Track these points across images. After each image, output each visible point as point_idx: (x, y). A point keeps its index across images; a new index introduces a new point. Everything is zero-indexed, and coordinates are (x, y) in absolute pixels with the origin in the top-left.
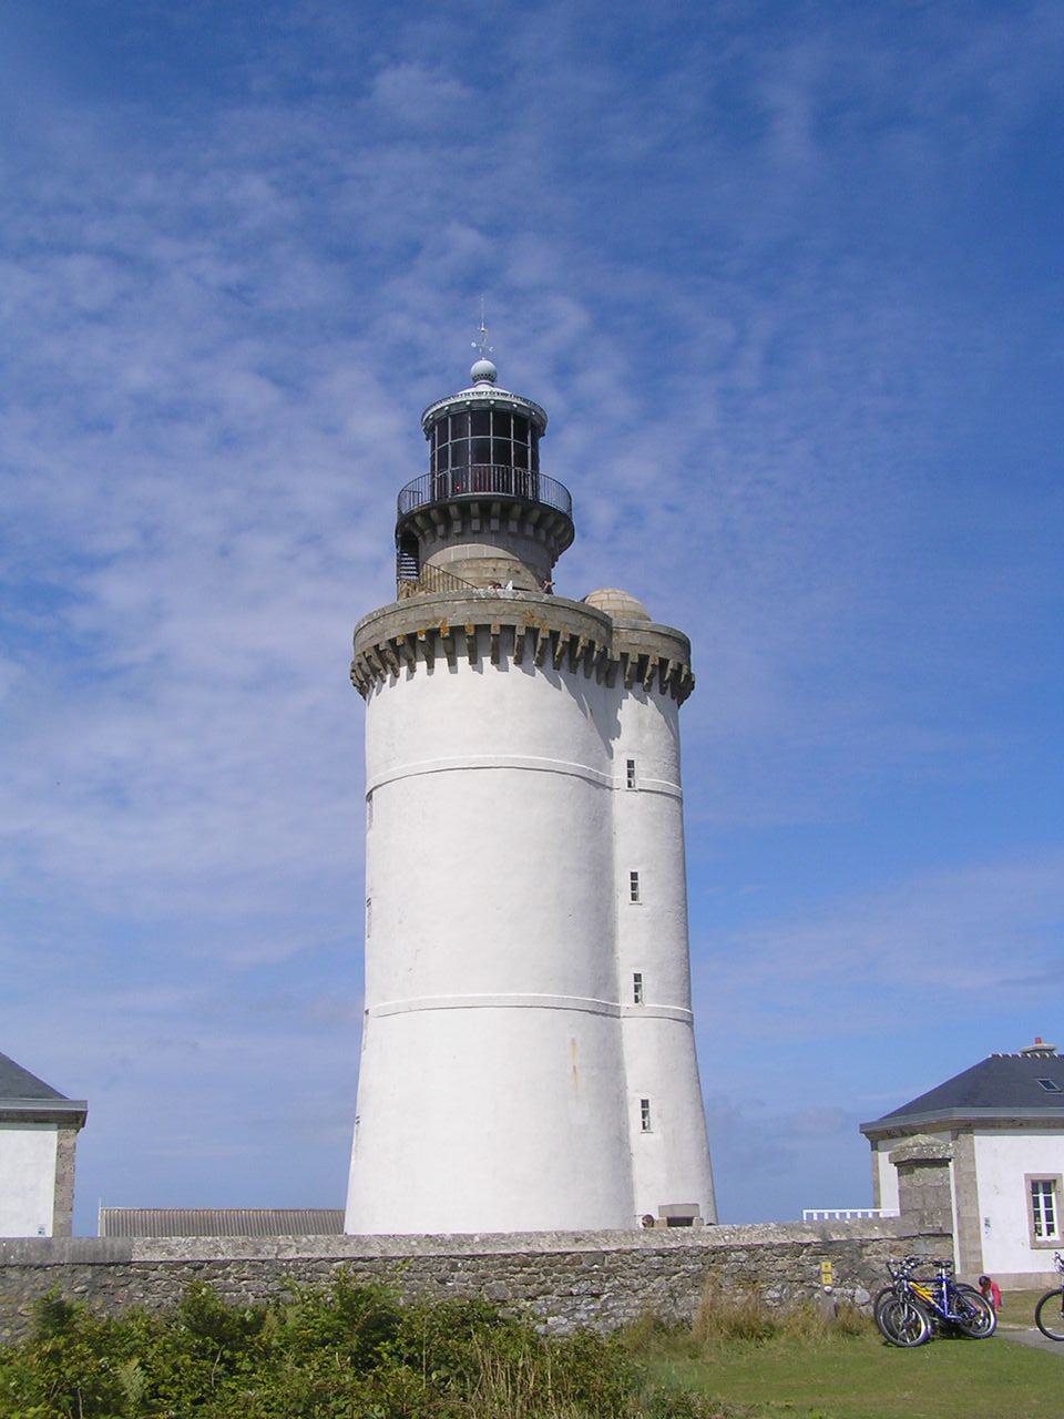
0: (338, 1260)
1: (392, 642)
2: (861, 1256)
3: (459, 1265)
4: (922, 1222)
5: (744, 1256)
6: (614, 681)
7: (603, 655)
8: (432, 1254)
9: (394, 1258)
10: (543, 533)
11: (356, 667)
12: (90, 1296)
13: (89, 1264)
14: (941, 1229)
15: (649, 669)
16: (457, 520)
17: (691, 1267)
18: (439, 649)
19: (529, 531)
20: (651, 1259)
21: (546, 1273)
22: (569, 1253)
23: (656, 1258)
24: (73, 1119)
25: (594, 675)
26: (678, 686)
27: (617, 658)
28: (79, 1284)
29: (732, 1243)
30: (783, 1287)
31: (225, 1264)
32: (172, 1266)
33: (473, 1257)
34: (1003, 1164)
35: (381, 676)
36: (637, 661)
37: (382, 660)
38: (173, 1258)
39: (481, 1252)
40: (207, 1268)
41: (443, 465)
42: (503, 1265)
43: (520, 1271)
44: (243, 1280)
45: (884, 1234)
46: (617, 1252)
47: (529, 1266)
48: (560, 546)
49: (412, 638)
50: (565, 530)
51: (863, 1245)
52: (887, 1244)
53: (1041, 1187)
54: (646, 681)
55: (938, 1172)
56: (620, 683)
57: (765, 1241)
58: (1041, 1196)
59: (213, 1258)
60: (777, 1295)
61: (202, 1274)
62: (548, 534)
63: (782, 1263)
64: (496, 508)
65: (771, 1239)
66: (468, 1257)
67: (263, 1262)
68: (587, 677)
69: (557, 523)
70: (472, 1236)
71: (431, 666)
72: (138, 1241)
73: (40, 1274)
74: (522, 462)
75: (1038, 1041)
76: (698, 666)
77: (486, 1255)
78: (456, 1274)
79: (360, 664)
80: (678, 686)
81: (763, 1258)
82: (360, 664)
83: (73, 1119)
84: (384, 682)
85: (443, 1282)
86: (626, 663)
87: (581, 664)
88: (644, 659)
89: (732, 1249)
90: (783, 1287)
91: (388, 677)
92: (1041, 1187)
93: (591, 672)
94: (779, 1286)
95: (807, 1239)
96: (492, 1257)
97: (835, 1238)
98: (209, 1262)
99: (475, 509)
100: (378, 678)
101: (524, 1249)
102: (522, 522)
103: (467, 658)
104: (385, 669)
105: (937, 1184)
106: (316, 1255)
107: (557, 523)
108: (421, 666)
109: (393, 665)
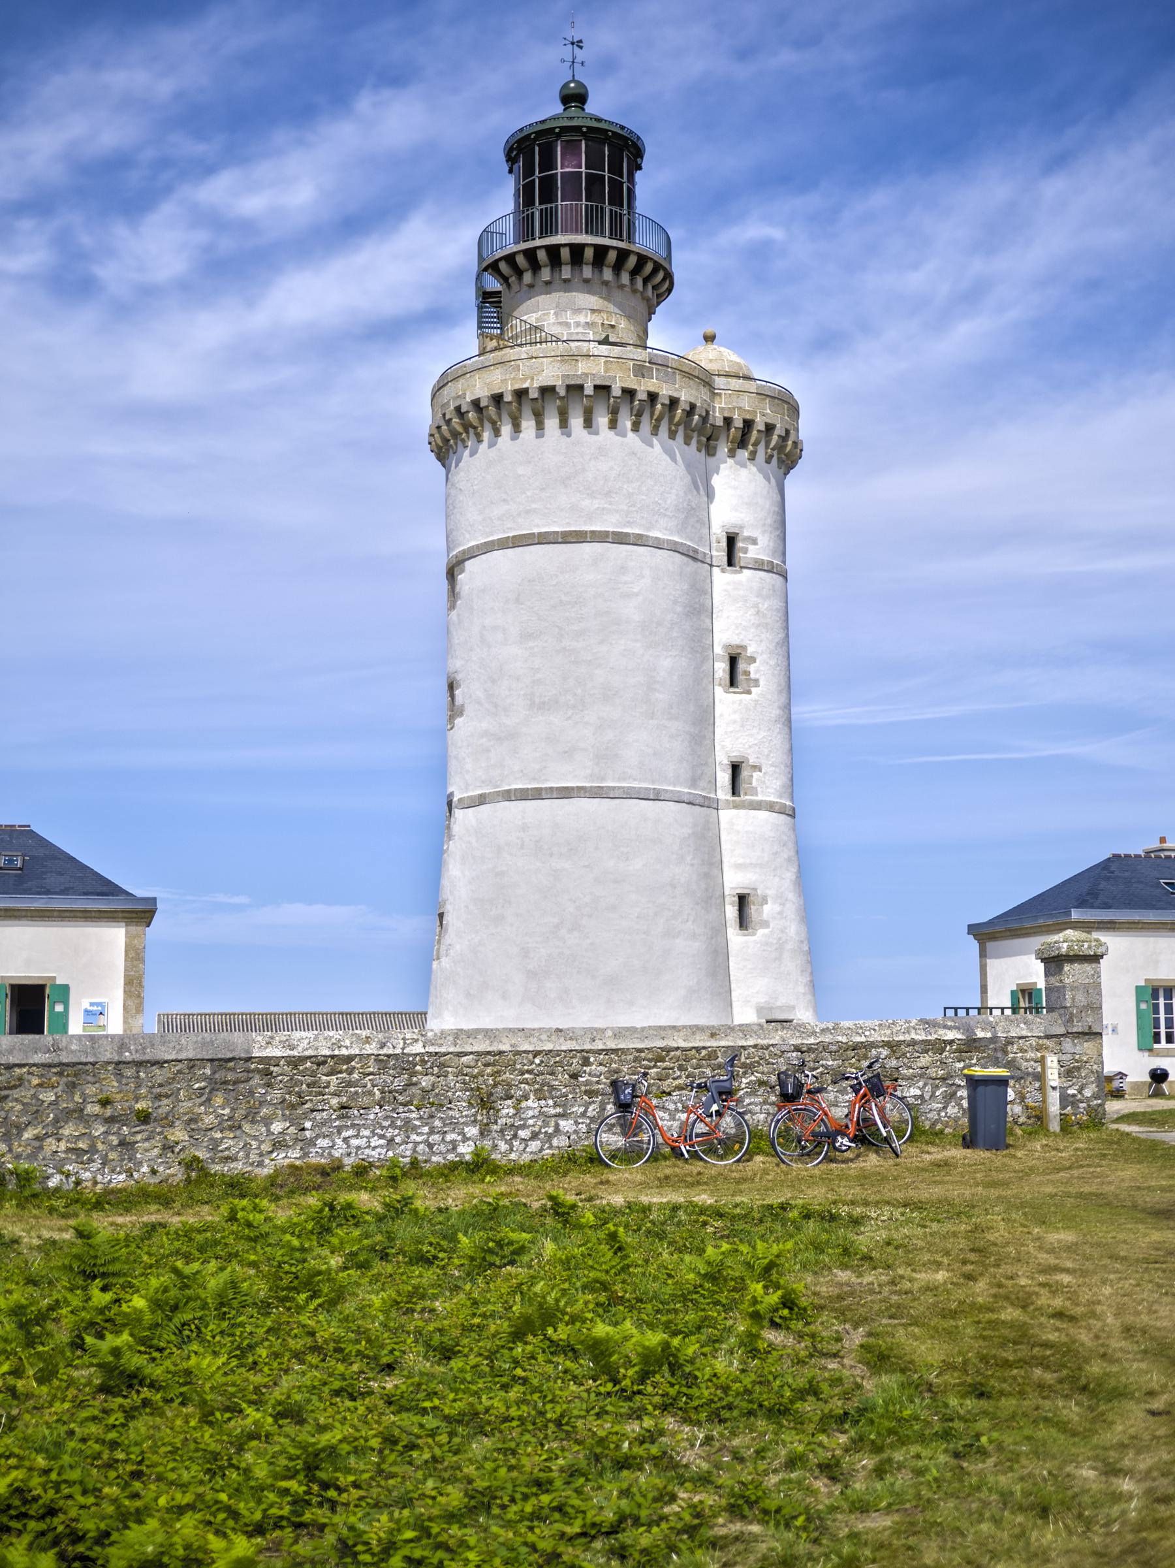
0: (466, 1054)
1: (476, 403)
2: (1006, 1053)
3: (592, 1059)
4: (1070, 1020)
5: (885, 1052)
6: (715, 448)
7: (705, 418)
8: (564, 1048)
9: (525, 1052)
10: (639, 281)
11: (435, 431)
12: (210, 1092)
13: (208, 1060)
14: (1090, 1027)
15: (754, 435)
16: (546, 266)
17: (830, 1063)
18: (527, 412)
19: (625, 278)
20: (789, 1054)
21: (681, 1068)
22: (704, 1048)
23: (794, 1054)
24: (141, 914)
25: (694, 442)
26: (785, 456)
27: (720, 422)
28: (198, 1081)
29: (872, 1039)
30: (925, 1085)
31: (350, 1058)
32: (295, 1062)
33: (607, 1051)
34: (1129, 961)
35: (463, 441)
36: (741, 426)
37: (458, 429)
38: (295, 1053)
39: (614, 1047)
40: (331, 1062)
41: (529, 202)
42: (636, 1059)
43: (655, 1066)
44: (369, 1074)
45: (1031, 1030)
46: (755, 1046)
47: (663, 1061)
48: (658, 296)
49: (497, 399)
50: (664, 279)
51: (1010, 1041)
52: (1033, 1042)
53: (1161, 993)
54: (751, 448)
55: (1088, 968)
56: (723, 449)
57: (907, 1038)
58: (1162, 1002)
59: (336, 1052)
60: (918, 1092)
61: (324, 1069)
62: (646, 281)
63: (924, 1060)
64: (589, 253)
65: (913, 1036)
66: (599, 1052)
67: (388, 1056)
68: (687, 443)
69: (655, 271)
70: (603, 1031)
71: (540, 426)
72: (259, 1038)
73: (156, 1070)
74: (616, 200)
75: (1163, 840)
76: (807, 429)
77: (618, 1050)
78: (587, 1069)
79: (439, 427)
80: (785, 456)
81: (904, 1054)
82: (439, 427)
83: (141, 914)
84: (480, 441)
85: (574, 1076)
86: (729, 430)
87: (681, 428)
88: (748, 424)
89: (872, 1045)
90: (925, 1085)
91: (486, 435)
92: (1161, 993)
93: (692, 438)
94: (921, 1084)
95: (950, 1035)
96: (624, 1051)
97: (980, 1034)
98: (333, 1057)
99: (565, 254)
100: (459, 443)
101: (660, 1044)
102: (618, 267)
103: (557, 421)
104: (467, 432)
105: (1087, 981)
106: (443, 1050)
107: (655, 271)
108: (506, 429)
109: (494, 423)
